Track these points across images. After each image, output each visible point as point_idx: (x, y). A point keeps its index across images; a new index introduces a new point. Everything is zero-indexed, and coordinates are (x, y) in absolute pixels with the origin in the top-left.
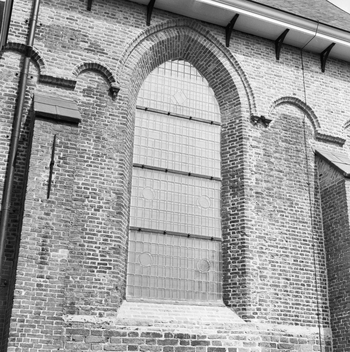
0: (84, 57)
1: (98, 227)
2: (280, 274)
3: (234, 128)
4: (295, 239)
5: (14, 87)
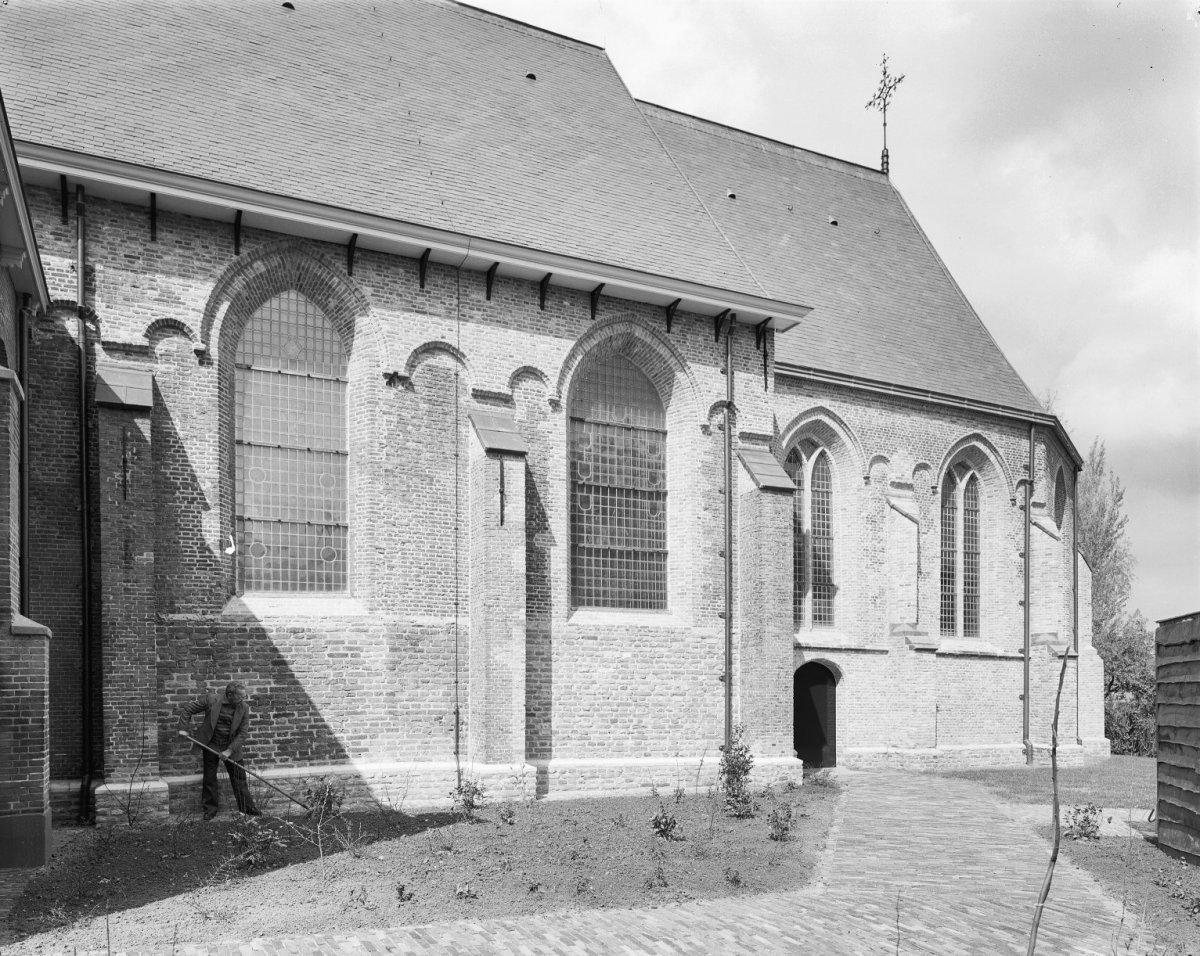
0: (154, 312)
1: (193, 521)
2: (412, 563)
3: (361, 388)
4: (433, 522)
5: (72, 359)
